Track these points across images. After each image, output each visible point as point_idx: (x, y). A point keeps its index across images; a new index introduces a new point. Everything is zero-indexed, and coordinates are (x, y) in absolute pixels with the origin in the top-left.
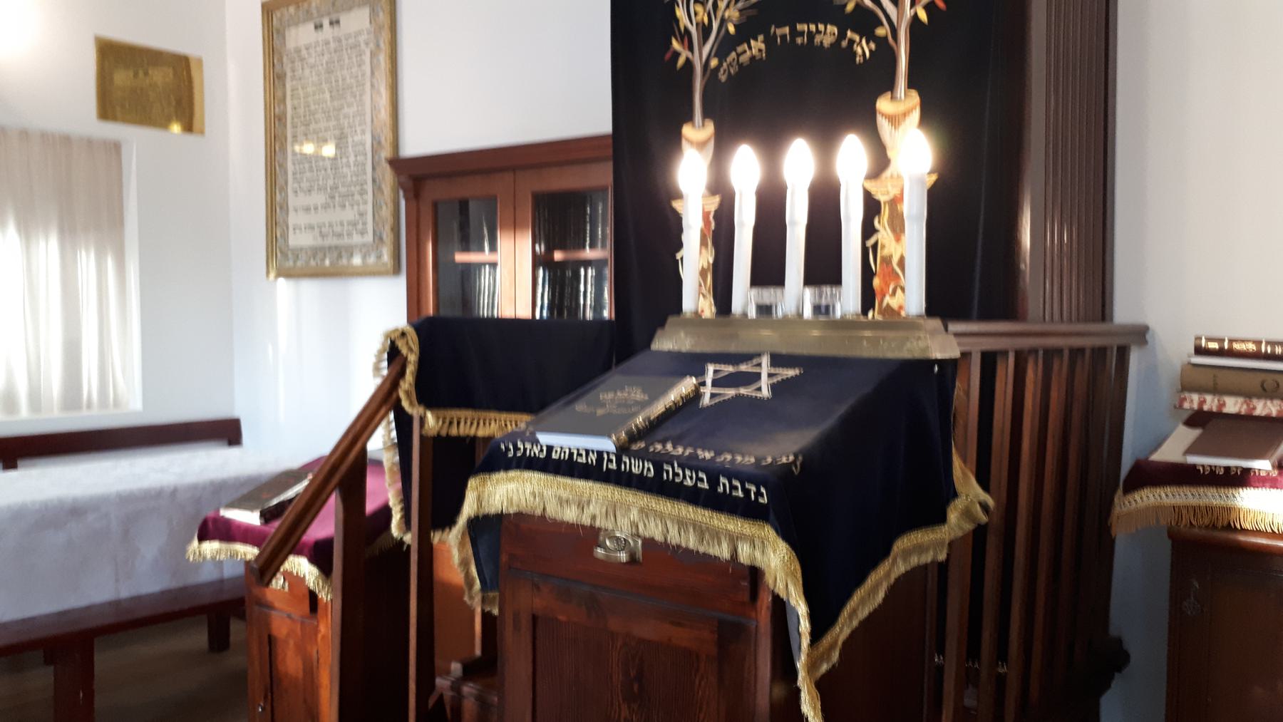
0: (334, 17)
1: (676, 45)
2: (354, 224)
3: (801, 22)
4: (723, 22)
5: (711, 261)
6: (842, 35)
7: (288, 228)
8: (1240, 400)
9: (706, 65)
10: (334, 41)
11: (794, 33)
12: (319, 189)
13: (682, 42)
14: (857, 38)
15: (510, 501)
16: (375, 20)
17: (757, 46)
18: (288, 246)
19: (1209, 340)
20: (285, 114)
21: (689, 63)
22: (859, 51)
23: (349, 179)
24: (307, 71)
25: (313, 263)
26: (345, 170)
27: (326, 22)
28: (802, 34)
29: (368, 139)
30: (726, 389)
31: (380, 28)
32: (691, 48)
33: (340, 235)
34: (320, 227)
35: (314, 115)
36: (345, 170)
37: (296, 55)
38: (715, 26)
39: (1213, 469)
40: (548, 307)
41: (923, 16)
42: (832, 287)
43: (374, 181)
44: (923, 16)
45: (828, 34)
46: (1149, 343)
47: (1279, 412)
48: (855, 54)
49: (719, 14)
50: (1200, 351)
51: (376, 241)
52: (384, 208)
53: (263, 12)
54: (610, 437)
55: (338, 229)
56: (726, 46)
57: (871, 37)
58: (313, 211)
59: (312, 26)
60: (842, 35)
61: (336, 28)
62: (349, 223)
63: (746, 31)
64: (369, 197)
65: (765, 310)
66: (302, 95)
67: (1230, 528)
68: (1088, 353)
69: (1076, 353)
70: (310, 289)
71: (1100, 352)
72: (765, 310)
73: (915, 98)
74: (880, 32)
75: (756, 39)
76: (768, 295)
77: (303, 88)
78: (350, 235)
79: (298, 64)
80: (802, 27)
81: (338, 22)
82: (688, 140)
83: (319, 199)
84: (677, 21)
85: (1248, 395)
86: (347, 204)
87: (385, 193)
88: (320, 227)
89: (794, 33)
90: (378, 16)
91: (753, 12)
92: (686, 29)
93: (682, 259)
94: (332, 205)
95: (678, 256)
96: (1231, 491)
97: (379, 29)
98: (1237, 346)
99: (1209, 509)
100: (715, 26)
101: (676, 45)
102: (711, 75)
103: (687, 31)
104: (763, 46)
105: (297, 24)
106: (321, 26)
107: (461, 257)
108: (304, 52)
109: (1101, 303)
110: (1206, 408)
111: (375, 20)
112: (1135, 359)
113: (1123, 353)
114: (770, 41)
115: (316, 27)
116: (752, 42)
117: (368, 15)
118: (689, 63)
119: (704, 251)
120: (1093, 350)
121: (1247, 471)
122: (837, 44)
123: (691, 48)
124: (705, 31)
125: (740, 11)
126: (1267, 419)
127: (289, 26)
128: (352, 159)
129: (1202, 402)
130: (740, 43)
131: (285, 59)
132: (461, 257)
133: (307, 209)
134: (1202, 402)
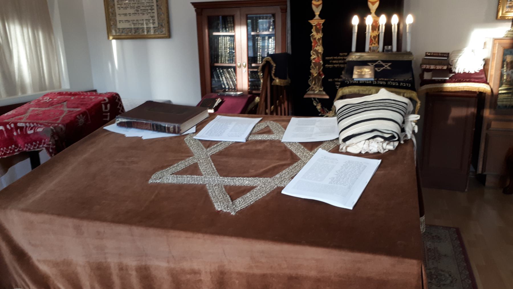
8: (434, 66)
15: (78, 229)
19: (429, 53)
25: (130, 34)
30: (353, 32)
39: (439, 80)
40: (362, 115)
42: (293, 151)
43: (157, 6)
47: (207, 111)
50: (427, 55)
54: (338, 89)
64: (155, 11)
67: (441, 91)
70: (128, 44)
83: (132, 11)
85: (436, 65)
87: (163, 9)
96: (442, 84)
98: (434, 54)
99: (438, 88)
107: (215, 34)
110: (427, 68)
121: (445, 80)
126: (439, 70)
129: (426, 67)
132: (215, 34)
134: (426, 67)
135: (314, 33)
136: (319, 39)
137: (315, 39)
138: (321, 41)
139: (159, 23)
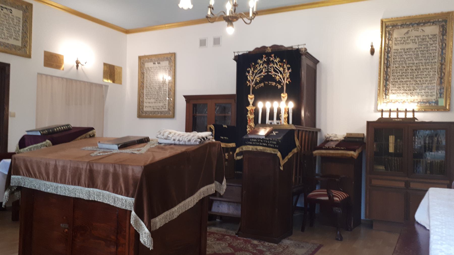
0: (159, 62)
1: (247, 82)
2: (163, 107)
3: (270, 81)
4: (256, 80)
5: (254, 117)
6: (276, 84)
7: (143, 107)
9: (253, 86)
10: (159, 67)
11: (268, 83)
12: (153, 98)
13: (248, 82)
14: (278, 85)
16: (170, 64)
17: (262, 84)
18: (143, 110)
20: (144, 81)
21: (250, 85)
22: (279, 87)
23: (162, 97)
24: (151, 73)
26: (161, 95)
27: (156, 63)
28: (270, 83)
29: (167, 89)
31: (172, 66)
32: (250, 83)
33: (158, 109)
34: (153, 107)
35: (152, 82)
36: (161, 95)
37: (147, 69)
38: (254, 80)
41: (288, 83)
44: (288, 83)
45: (274, 84)
46: (320, 61)
48: (278, 87)
49: (255, 78)
51: (169, 110)
52: (171, 103)
53: (139, 59)
55: (158, 107)
56: (256, 84)
57: (280, 85)
58: (151, 103)
59: (152, 63)
60: (276, 84)
61: (159, 64)
62: (161, 106)
63: (261, 82)
65: (278, 123)
66: (149, 78)
68: (311, 132)
69: (310, 132)
71: (313, 132)
72: (271, 123)
73: (286, 94)
74: (282, 84)
75: (262, 83)
76: (279, 121)
77: (149, 76)
78: (161, 109)
79: (148, 71)
80: (270, 82)
81: (160, 63)
82: (249, 97)
84: (248, 78)
86: (161, 102)
88: (153, 107)
89: (268, 83)
90: (171, 63)
91: (262, 79)
92: (249, 80)
93: (281, 116)
94: (156, 102)
95: (280, 115)
97: (171, 66)
100: (254, 80)
101: (247, 82)
102: (254, 88)
103: (249, 80)
104: (263, 85)
105: (148, 62)
106: (155, 63)
108: (150, 69)
109: (314, 124)
111: (170, 64)
112: (319, 134)
113: (317, 133)
114: (264, 84)
115: (154, 63)
116: (262, 84)
117: (168, 63)
118: (250, 85)
119: (285, 115)
120: (312, 131)
122: (275, 85)
123: (250, 83)
124: (253, 81)
125: (260, 79)
127: (146, 62)
128: (163, 93)
130: (260, 83)
131: (144, 69)
133: (149, 103)
135: (249, 115)
136: (252, 119)
137: (250, 118)
138: (253, 120)
139: (168, 109)
